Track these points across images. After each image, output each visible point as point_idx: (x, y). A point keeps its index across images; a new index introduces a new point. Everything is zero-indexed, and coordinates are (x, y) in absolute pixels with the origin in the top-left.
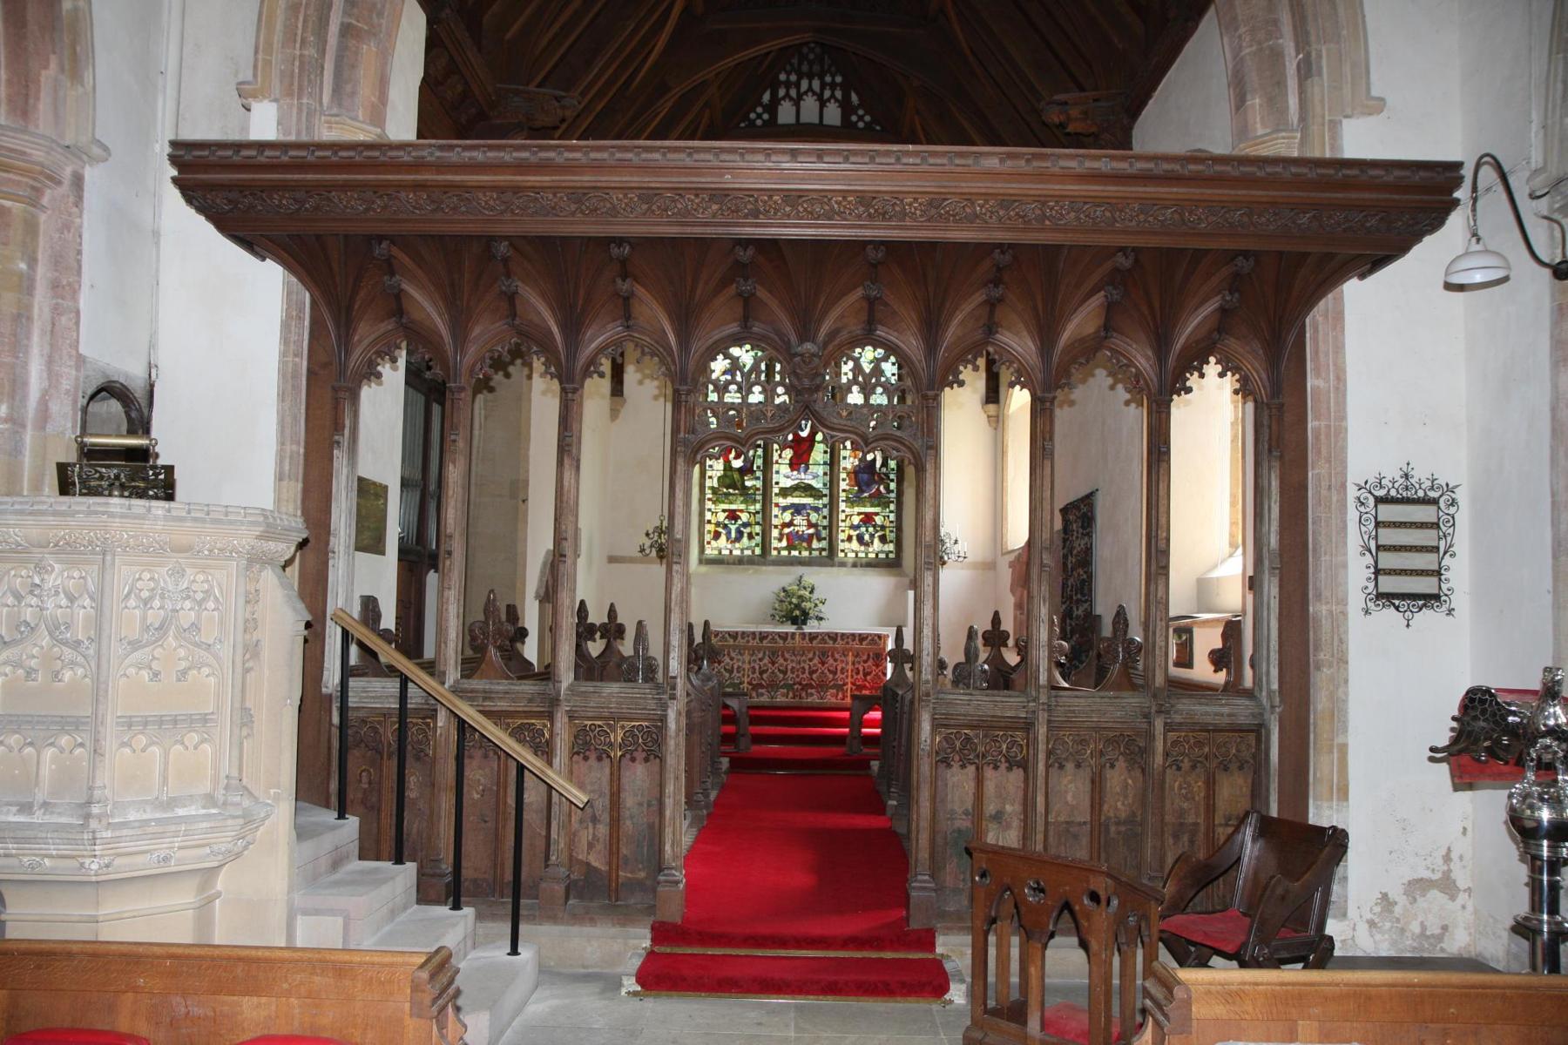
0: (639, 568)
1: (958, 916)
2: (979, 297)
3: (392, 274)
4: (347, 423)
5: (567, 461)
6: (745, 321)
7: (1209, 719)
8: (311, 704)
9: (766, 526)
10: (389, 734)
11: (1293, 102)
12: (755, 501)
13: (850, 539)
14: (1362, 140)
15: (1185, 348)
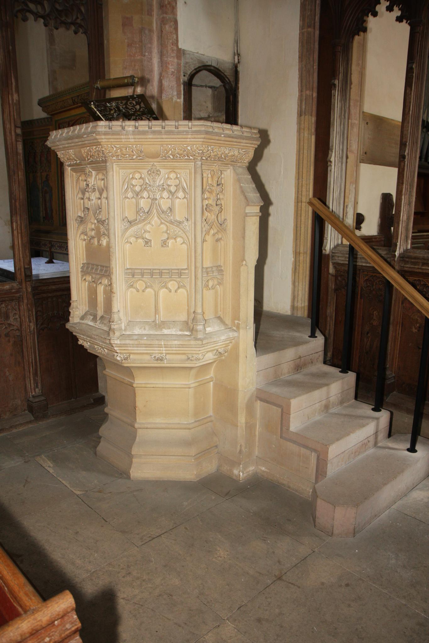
4: (341, 70)
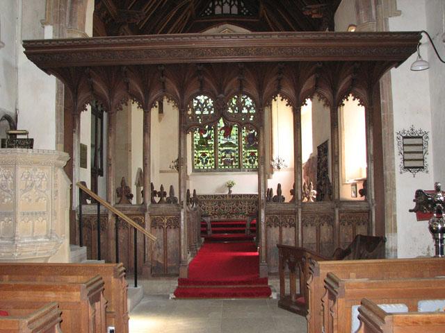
0: (172, 174)
1: (275, 274)
2: (274, 78)
3: (90, 77)
5: (146, 135)
6: (201, 88)
7: (353, 209)
8: (72, 213)
9: (216, 157)
10: (94, 222)
11: (374, 12)
12: (212, 149)
13: (246, 162)
14: (396, 25)
15: (341, 91)
